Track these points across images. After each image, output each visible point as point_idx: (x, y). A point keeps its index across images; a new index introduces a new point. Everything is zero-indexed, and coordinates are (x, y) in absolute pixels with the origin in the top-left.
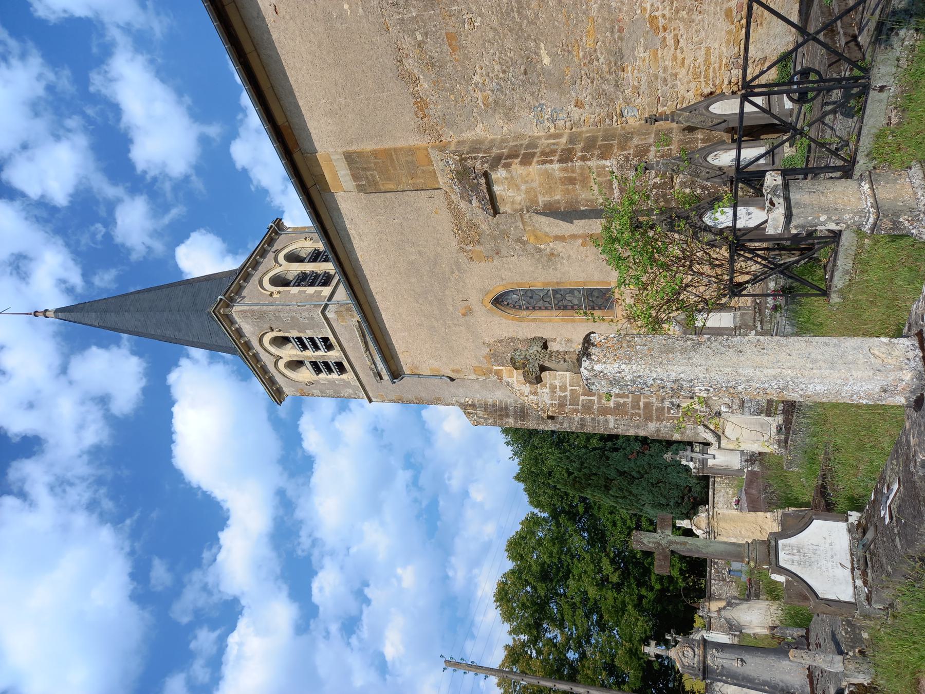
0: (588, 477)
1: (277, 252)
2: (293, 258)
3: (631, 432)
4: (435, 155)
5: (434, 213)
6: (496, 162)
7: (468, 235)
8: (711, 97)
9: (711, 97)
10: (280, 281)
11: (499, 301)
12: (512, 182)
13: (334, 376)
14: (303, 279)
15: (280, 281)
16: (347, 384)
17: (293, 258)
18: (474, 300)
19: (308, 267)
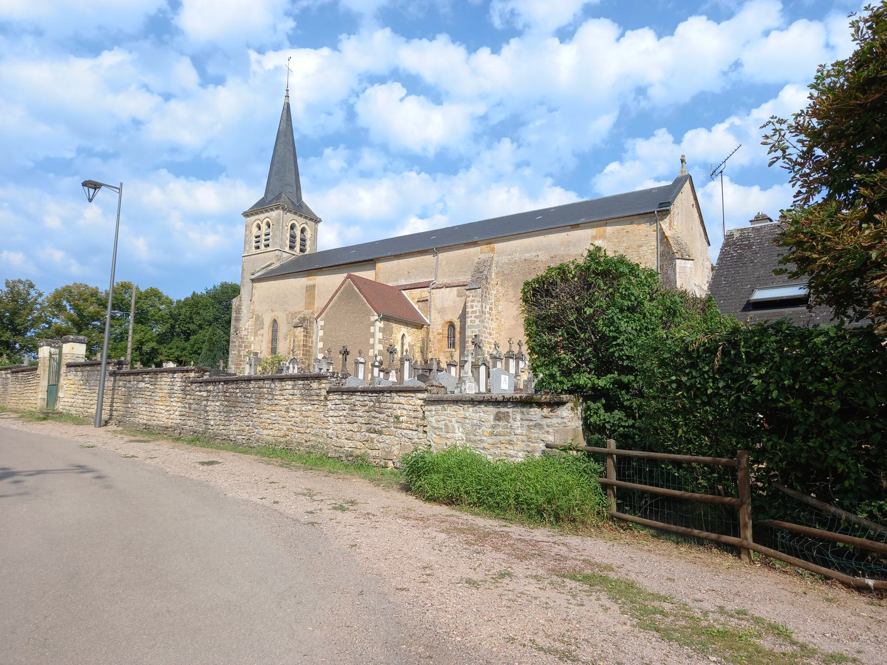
0: (213, 344)
1: (306, 223)
2: (303, 231)
3: (230, 359)
4: (311, 311)
5: (299, 307)
6: (306, 328)
7: (293, 315)
8: (173, 371)
9: (173, 371)
10: (293, 227)
11: (275, 321)
12: (300, 332)
13: (254, 244)
14: (293, 237)
15: (293, 227)
16: (251, 248)
17: (303, 231)
18: (276, 313)
19: (298, 239)
